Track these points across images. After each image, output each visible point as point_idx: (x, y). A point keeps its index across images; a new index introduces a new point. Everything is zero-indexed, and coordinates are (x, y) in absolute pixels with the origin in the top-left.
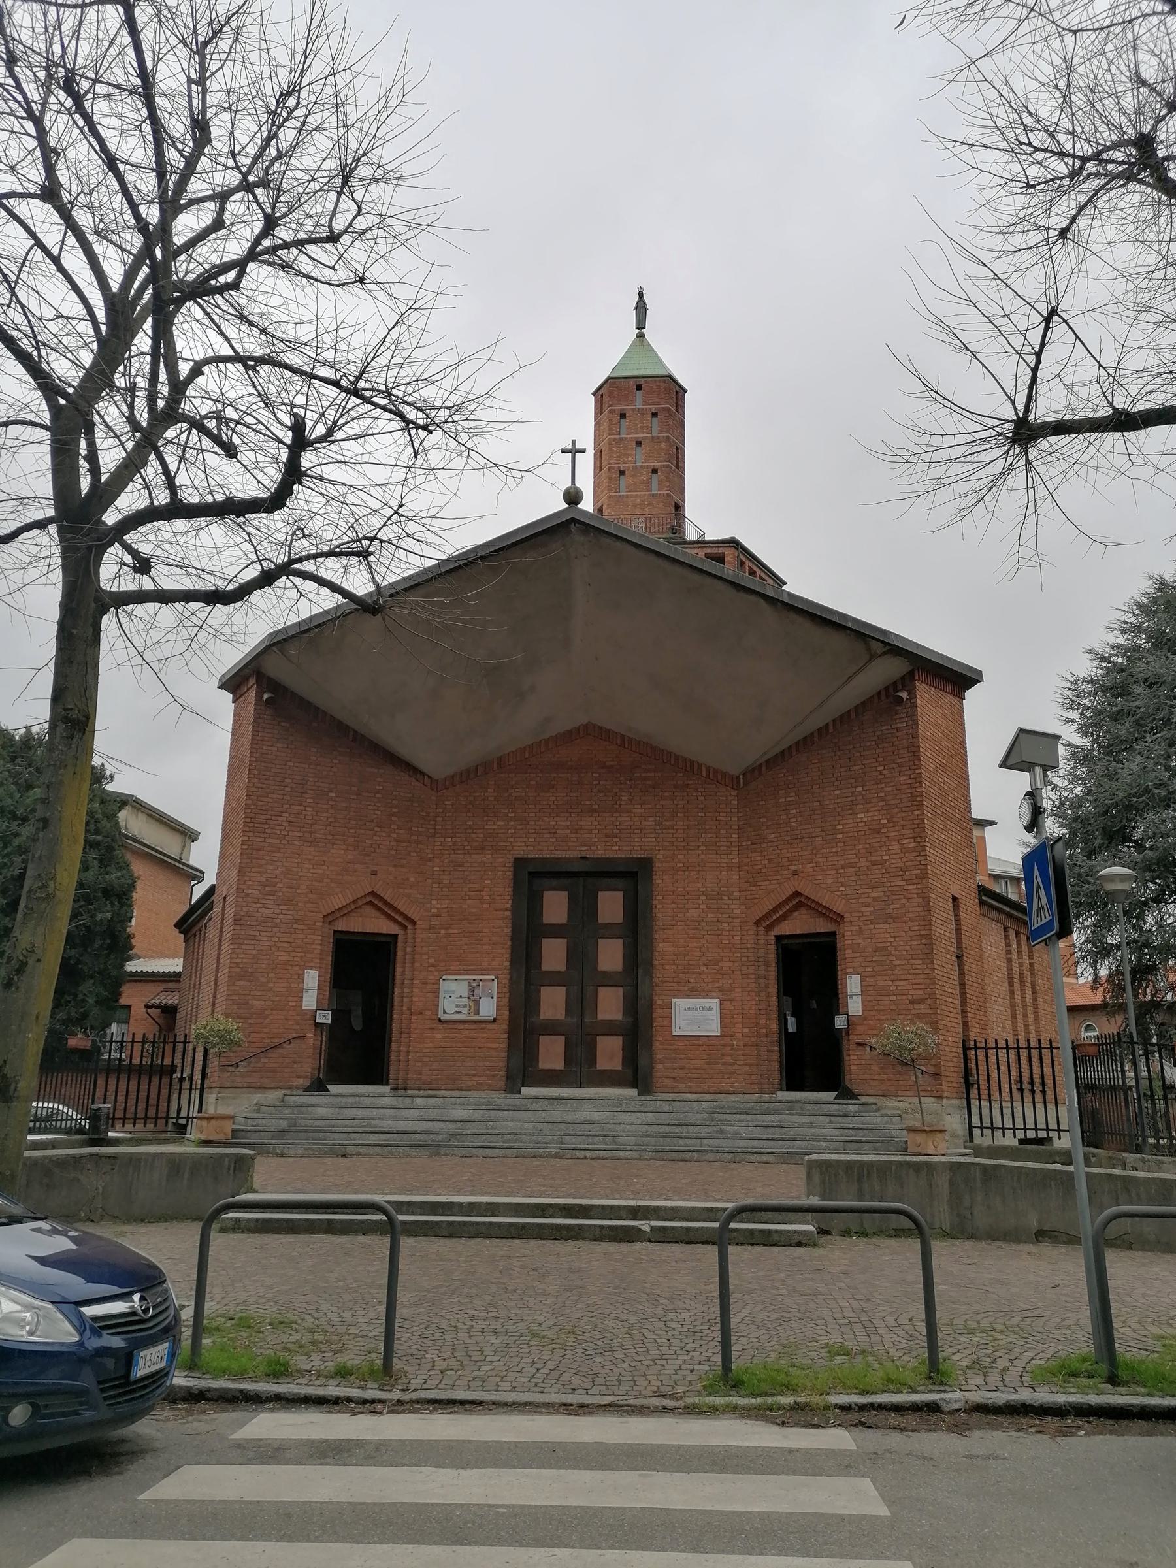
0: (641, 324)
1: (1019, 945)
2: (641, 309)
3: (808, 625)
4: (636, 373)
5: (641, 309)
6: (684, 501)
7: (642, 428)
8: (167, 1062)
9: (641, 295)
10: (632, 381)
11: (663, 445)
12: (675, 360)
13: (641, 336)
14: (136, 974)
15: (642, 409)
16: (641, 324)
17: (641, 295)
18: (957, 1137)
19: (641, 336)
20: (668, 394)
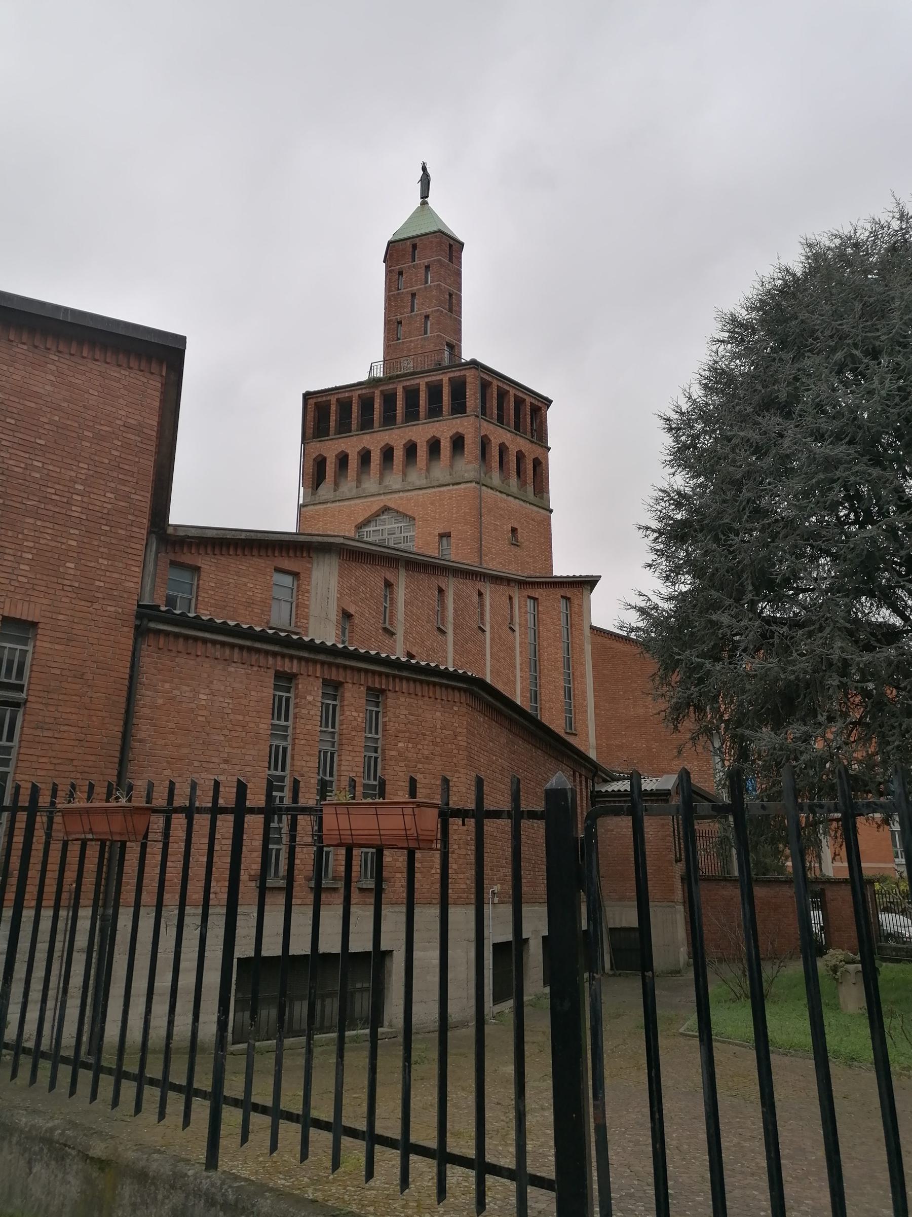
0: (425, 194)
1: (581, 782)
2: (425, 181)
3: (148, 463)
4: (411, 234)
5: (425, 181)
6: (460, 341)
7: (416, 281)
8: (361, 943)
9: (424, 169)
10: (408, 243)
11: (434, 293)
12: (451, 215)
13: (424, 203)
14: (373, 848)
15: (423, 265)
16: (425, 194)
17: (424, 169)
18: (827, 1005)
19: (424, 203)
20: (451, 248)
